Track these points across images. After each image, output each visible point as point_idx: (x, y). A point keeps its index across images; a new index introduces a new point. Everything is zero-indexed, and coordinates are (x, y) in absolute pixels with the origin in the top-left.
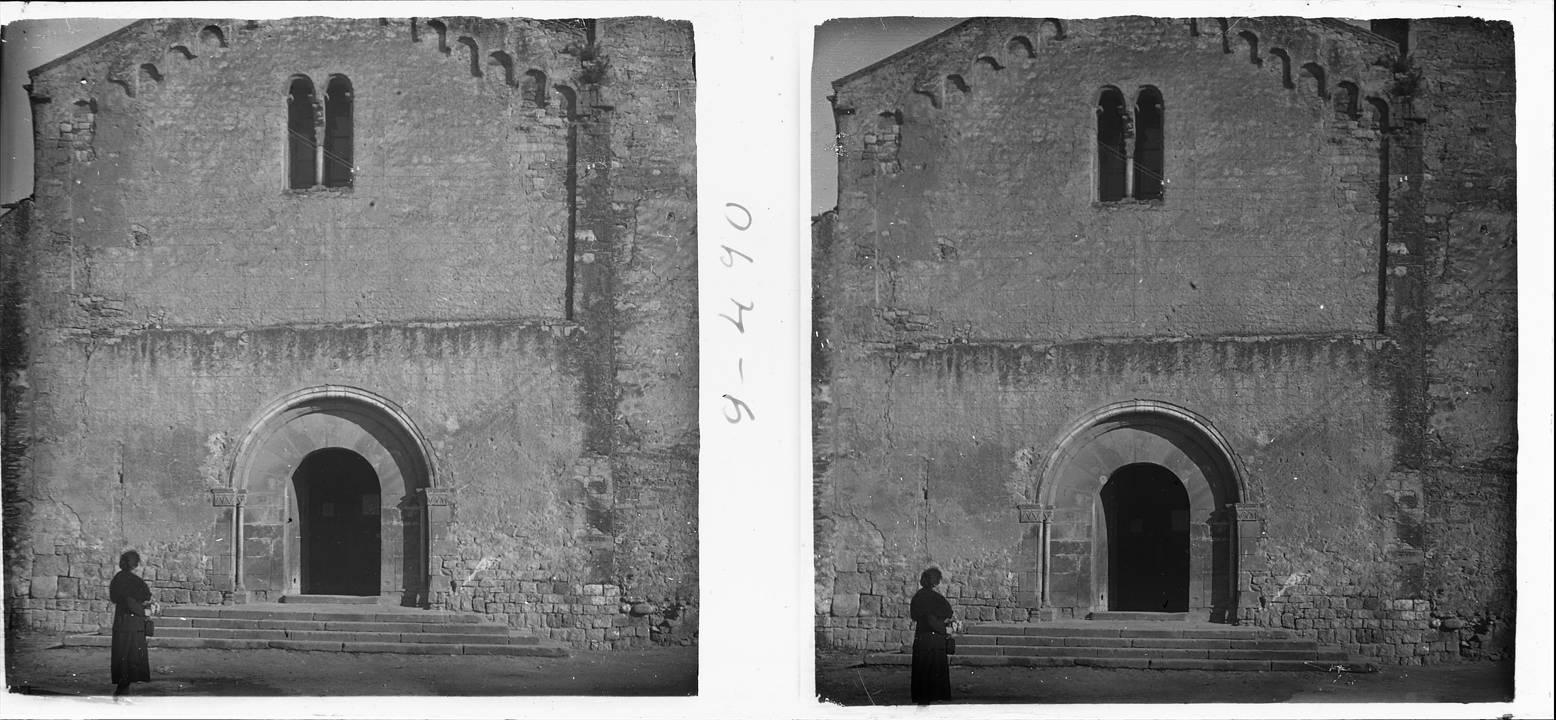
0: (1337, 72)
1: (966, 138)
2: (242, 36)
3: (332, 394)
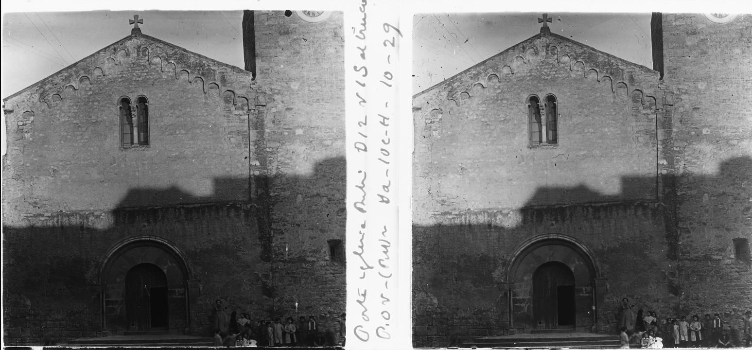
0: (225, 86)
1: (471, 120)
2: (99, 80)
3: (551, 237)
